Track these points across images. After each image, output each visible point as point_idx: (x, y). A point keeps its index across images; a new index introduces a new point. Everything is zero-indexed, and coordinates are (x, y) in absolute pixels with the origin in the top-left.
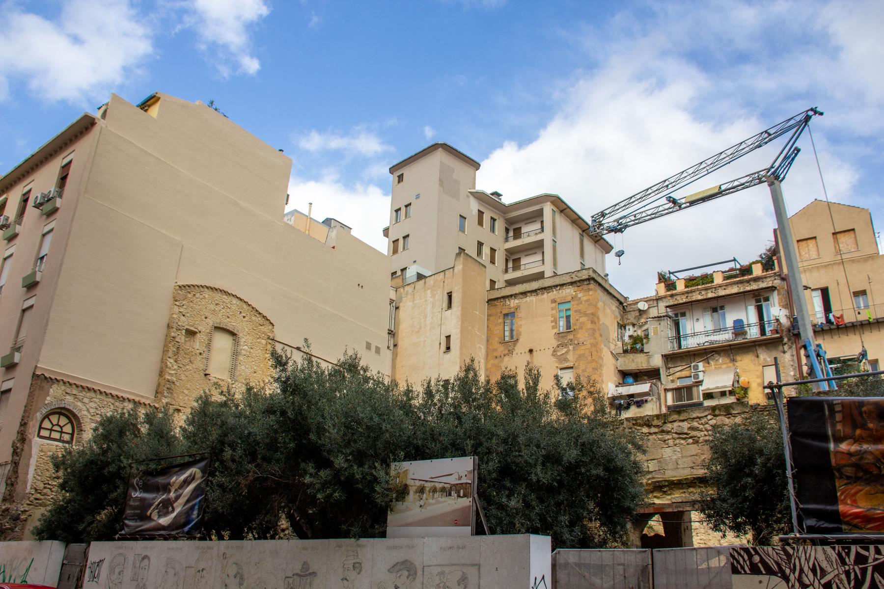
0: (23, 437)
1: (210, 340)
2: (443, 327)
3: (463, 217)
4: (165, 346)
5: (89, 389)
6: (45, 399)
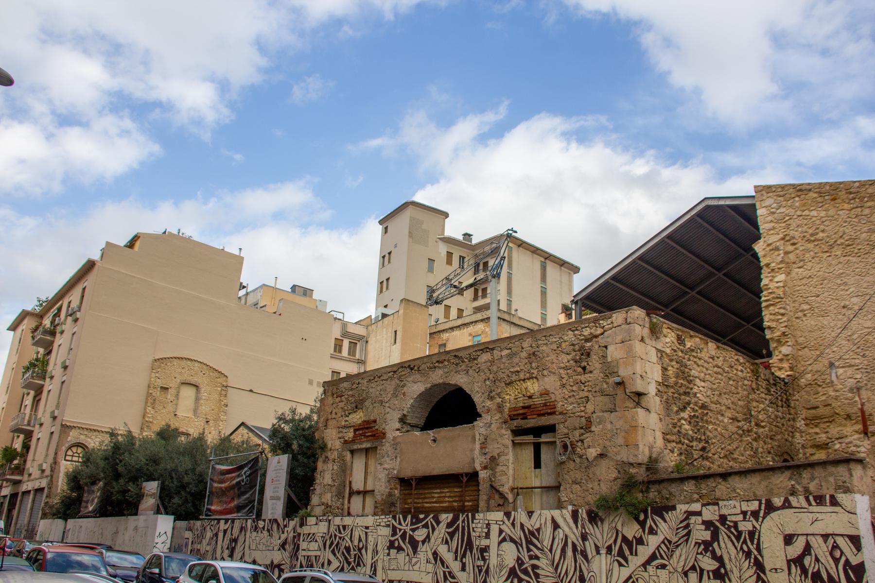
0: (55, 462)
1: (178, 392)
2: (391, 358)
3: (431, 261)
4: (147, 399)
5: (95, 430)
6: (67, 438)
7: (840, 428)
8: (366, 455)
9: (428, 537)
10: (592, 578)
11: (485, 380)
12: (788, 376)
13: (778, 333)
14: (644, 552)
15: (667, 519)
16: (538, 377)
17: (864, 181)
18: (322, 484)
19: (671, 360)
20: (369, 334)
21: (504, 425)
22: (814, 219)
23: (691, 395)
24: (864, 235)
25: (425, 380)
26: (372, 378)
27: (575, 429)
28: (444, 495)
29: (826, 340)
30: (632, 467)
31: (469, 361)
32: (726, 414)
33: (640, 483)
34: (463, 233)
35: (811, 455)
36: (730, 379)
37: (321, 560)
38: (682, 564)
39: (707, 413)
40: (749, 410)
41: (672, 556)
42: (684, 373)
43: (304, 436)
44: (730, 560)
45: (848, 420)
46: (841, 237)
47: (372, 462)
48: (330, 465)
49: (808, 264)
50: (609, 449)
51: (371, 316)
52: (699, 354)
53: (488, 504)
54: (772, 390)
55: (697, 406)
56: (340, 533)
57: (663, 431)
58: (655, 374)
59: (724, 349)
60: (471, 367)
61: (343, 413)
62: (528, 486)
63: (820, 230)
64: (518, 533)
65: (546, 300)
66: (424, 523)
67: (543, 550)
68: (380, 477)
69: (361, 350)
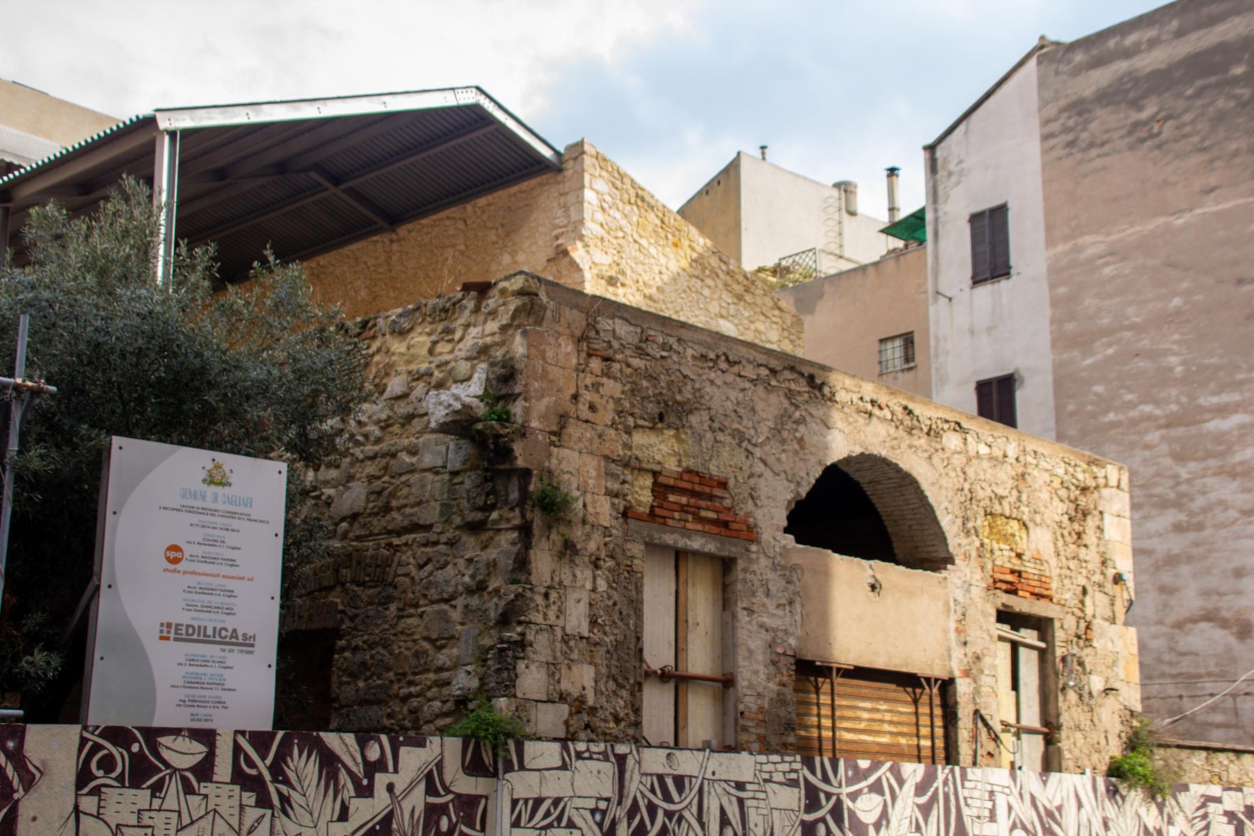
56: (668, 798)
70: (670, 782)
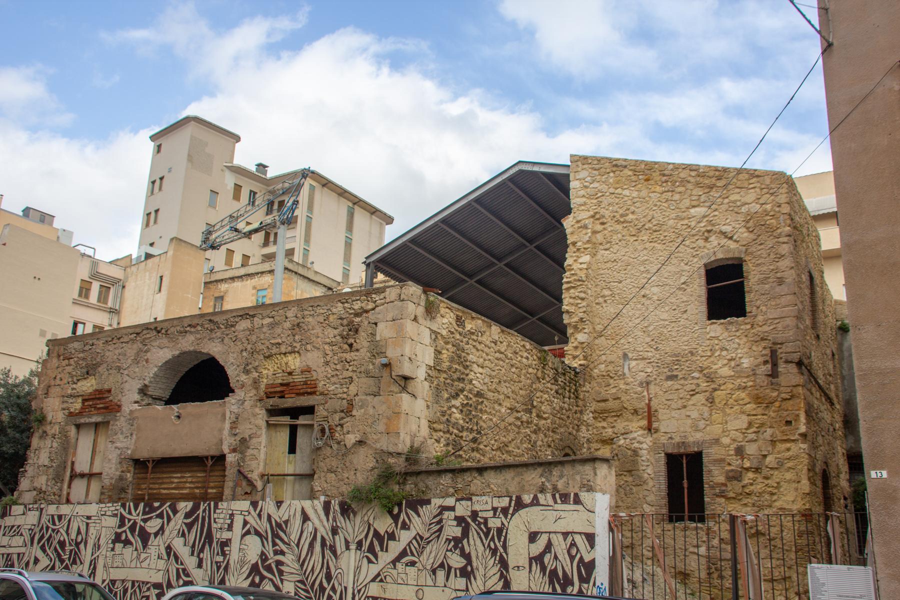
2: (153, 309)
7: (626, 423)
8: (96, 430)
9: (162, 529)
10: (339, 575)
11: (242, 351)
12: (581, 365)
13: (576, 319)
14: (395, 548)
15: (421, 513)
16: (301, 351)
17: (678, 164)
18: (36, 465)
19: (447, 343)
20: (127, 278)
21: (258, 403)
22: (626, 198)
23: (466, 382)
24: (671, 222)
25: (173, 346)
26: (110, 339)
27: (336, 412)
28: (185, 480)
29: (623, 330)
30: (391, 456)
31: (226, 328)
32: (504, 404)
33: (397, 474)
34: (256, 163)
35: (597, 450)
36: (512, 366)
37: (26, 559)
38: (431, 561)
39: (482, 402)
40: (531, 400)
41: (422, 552)
42: (460, 357)
43: (18, 405)
44: (477, 557)
45: (635, 415)
46: (650, 221)
47: (101, 440)
48: (48, 442)
49: (614, 247)
50: (369, 435)
51: (131, 255)
52: (479, 338)
53: (234, 492)
54: (560, 379)
55: (471, 393)
56: (54, 524)
57: (429, 419)
58: (428, 357)
59: (509, 333)
60: (227, 335)
61: (70, 380)
62: (279, 473)
63: (630, 211)
64: (265, 525)
65: (350, 253)
66: (158, 512)
67: (289, 545)
68: (110, 457)
69: (116, 297)
70: (56, 518)
